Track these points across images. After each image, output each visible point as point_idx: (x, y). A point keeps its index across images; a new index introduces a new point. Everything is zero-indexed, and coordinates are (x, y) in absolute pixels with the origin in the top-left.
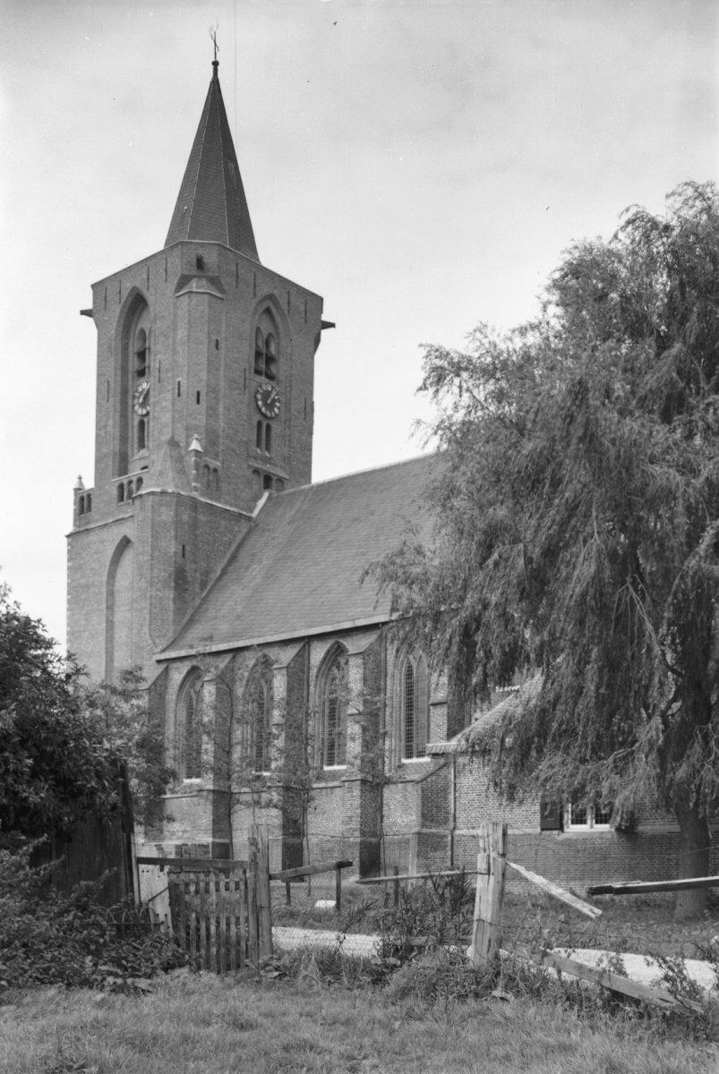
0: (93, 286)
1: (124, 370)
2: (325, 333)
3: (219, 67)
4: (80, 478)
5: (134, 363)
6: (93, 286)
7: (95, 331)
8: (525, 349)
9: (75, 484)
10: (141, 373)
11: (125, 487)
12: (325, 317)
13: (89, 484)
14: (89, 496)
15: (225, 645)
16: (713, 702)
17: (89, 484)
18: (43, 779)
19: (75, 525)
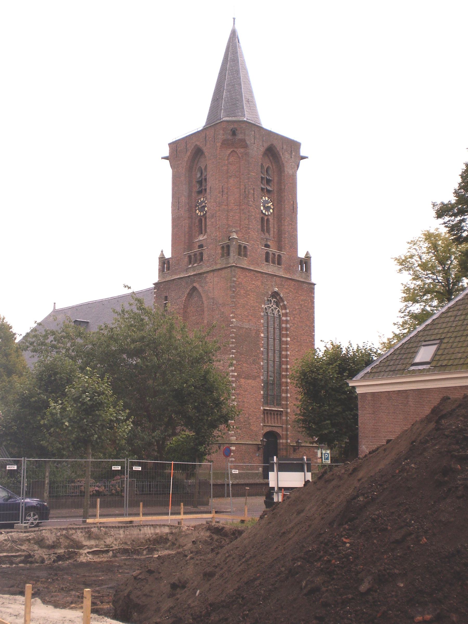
0: (170, 144)
1: (190, 192)
2: (302, 162)
3: (235, 20)
4: (162, 251)
5: (196, 188)
6: (170, 144)
7: (171, 170)
8: (86, 539)
9: (158, 255)
10: (200, 192)
11: (193, 257)
12: (302, 153)
13: (168, 255)
14: (168, 262)
15: (242, 480)
16: (433, 349)
17: (168, 255)
18: (36, 538)
19: (159, 276)
